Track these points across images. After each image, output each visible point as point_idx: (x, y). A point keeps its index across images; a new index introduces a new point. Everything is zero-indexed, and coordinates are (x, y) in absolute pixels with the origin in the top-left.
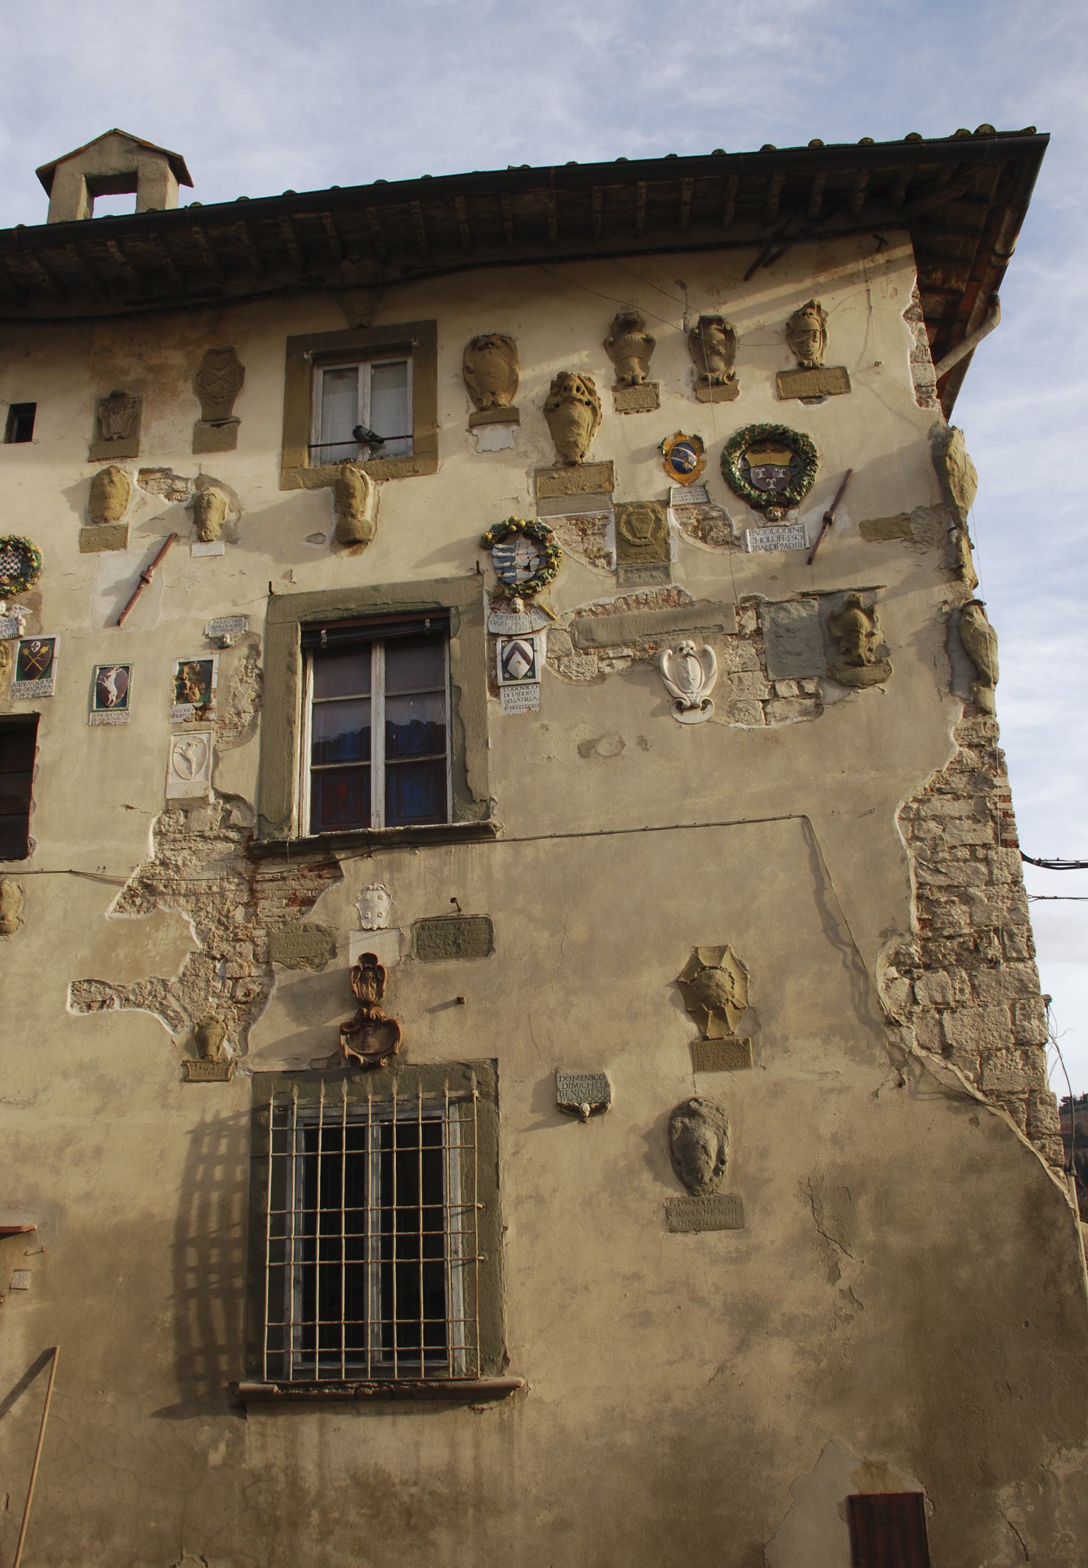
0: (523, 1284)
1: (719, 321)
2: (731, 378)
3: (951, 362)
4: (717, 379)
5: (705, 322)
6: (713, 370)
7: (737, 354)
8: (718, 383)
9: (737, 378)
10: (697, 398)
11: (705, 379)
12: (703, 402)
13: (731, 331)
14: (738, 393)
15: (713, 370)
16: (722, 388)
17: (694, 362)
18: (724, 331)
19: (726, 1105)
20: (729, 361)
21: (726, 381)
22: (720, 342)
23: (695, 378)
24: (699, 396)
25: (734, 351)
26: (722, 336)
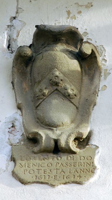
0: (67, 22)
1: (72, 37)
2: (83, 141)
3: (17, 103)
4: (56, 142)
5: (46, 37)
6: (50, 126)
7: (102, 99)
8: (57, 149)
9: (94, 141)
10: (14, 174)
11: (33, 140)
12: (23, 182)
13: (93, 56)
14: (92, 170)
15: (50, 126)
16: (64, 158)
17: (19, 108)
18: (81, 57)
19: (44, 58)
20: (84, 110)
21: (73, 146)
22: (69, 74)
23: (18, 137)
24: (20, 172)
25: (95, 93)
26: (74, 65)
